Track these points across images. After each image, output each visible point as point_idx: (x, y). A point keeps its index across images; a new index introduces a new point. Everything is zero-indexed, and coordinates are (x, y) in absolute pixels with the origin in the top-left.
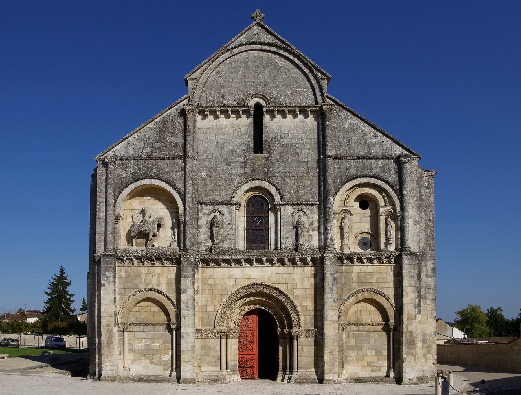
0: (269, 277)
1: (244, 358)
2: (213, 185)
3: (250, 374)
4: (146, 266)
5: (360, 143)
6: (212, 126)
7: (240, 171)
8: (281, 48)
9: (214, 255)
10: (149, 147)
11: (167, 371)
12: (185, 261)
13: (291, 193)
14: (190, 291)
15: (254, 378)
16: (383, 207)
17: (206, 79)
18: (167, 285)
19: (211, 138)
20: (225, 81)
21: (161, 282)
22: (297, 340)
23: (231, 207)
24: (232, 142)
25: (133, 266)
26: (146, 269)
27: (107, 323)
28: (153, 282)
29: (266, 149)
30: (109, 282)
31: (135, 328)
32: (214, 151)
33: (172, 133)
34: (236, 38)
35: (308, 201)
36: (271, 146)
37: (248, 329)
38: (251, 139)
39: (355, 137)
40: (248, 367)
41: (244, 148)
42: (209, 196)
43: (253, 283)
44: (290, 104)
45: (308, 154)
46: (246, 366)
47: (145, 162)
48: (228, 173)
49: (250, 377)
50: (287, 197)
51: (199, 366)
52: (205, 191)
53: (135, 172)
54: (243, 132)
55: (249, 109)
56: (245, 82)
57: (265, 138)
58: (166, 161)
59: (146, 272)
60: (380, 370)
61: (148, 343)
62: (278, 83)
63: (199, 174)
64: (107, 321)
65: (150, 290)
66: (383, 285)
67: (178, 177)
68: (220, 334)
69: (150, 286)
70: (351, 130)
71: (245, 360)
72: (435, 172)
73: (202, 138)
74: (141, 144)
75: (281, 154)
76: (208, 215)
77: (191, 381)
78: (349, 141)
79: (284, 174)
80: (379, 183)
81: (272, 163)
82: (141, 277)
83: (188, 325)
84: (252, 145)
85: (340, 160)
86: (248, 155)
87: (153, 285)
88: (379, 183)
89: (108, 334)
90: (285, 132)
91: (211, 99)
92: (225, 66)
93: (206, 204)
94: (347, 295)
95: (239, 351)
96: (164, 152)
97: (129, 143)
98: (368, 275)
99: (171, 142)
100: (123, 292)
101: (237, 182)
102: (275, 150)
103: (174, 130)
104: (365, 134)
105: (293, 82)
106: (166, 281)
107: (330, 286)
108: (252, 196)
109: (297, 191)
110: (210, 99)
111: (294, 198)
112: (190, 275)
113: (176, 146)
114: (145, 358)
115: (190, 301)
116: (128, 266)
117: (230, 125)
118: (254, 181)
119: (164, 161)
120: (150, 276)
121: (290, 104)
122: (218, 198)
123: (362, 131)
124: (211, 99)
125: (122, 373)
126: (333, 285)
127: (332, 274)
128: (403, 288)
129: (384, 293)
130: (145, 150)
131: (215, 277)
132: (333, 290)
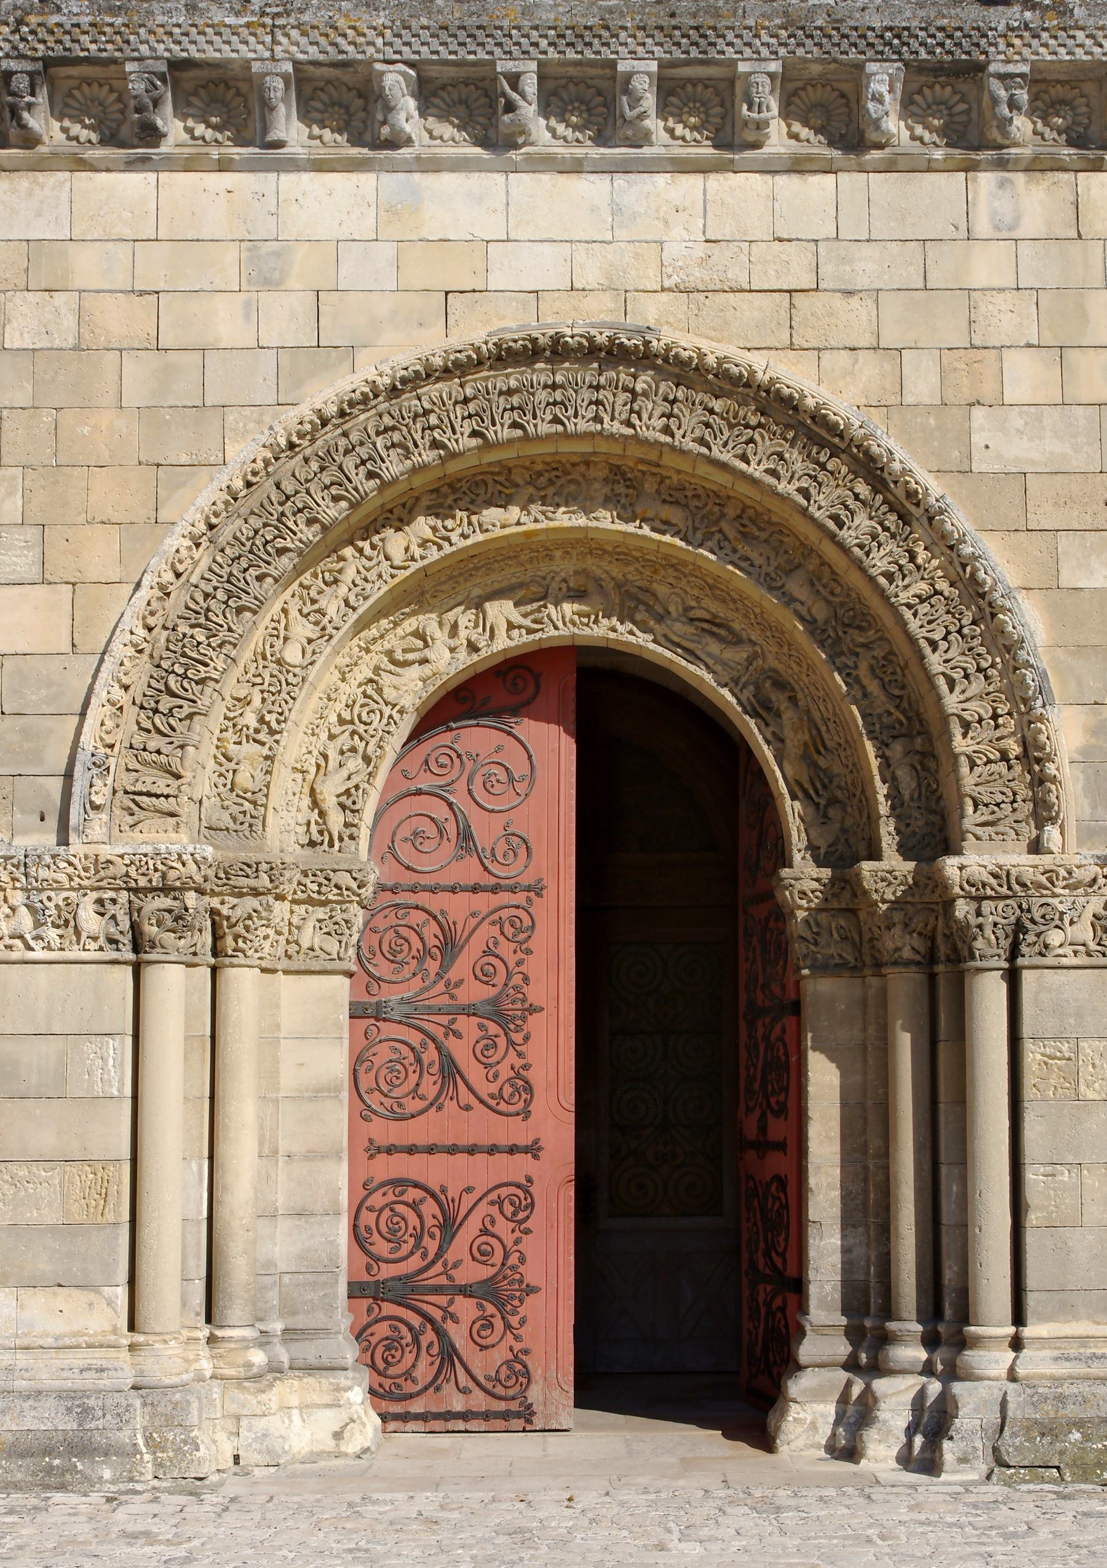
0: (698, 276)
1: (413, 1194)
3: (483, 1363)
37: (469, 871)
46: (434, 1276)
49: (479, 1401)
71: (430, 1208)
95: (362, 1113)
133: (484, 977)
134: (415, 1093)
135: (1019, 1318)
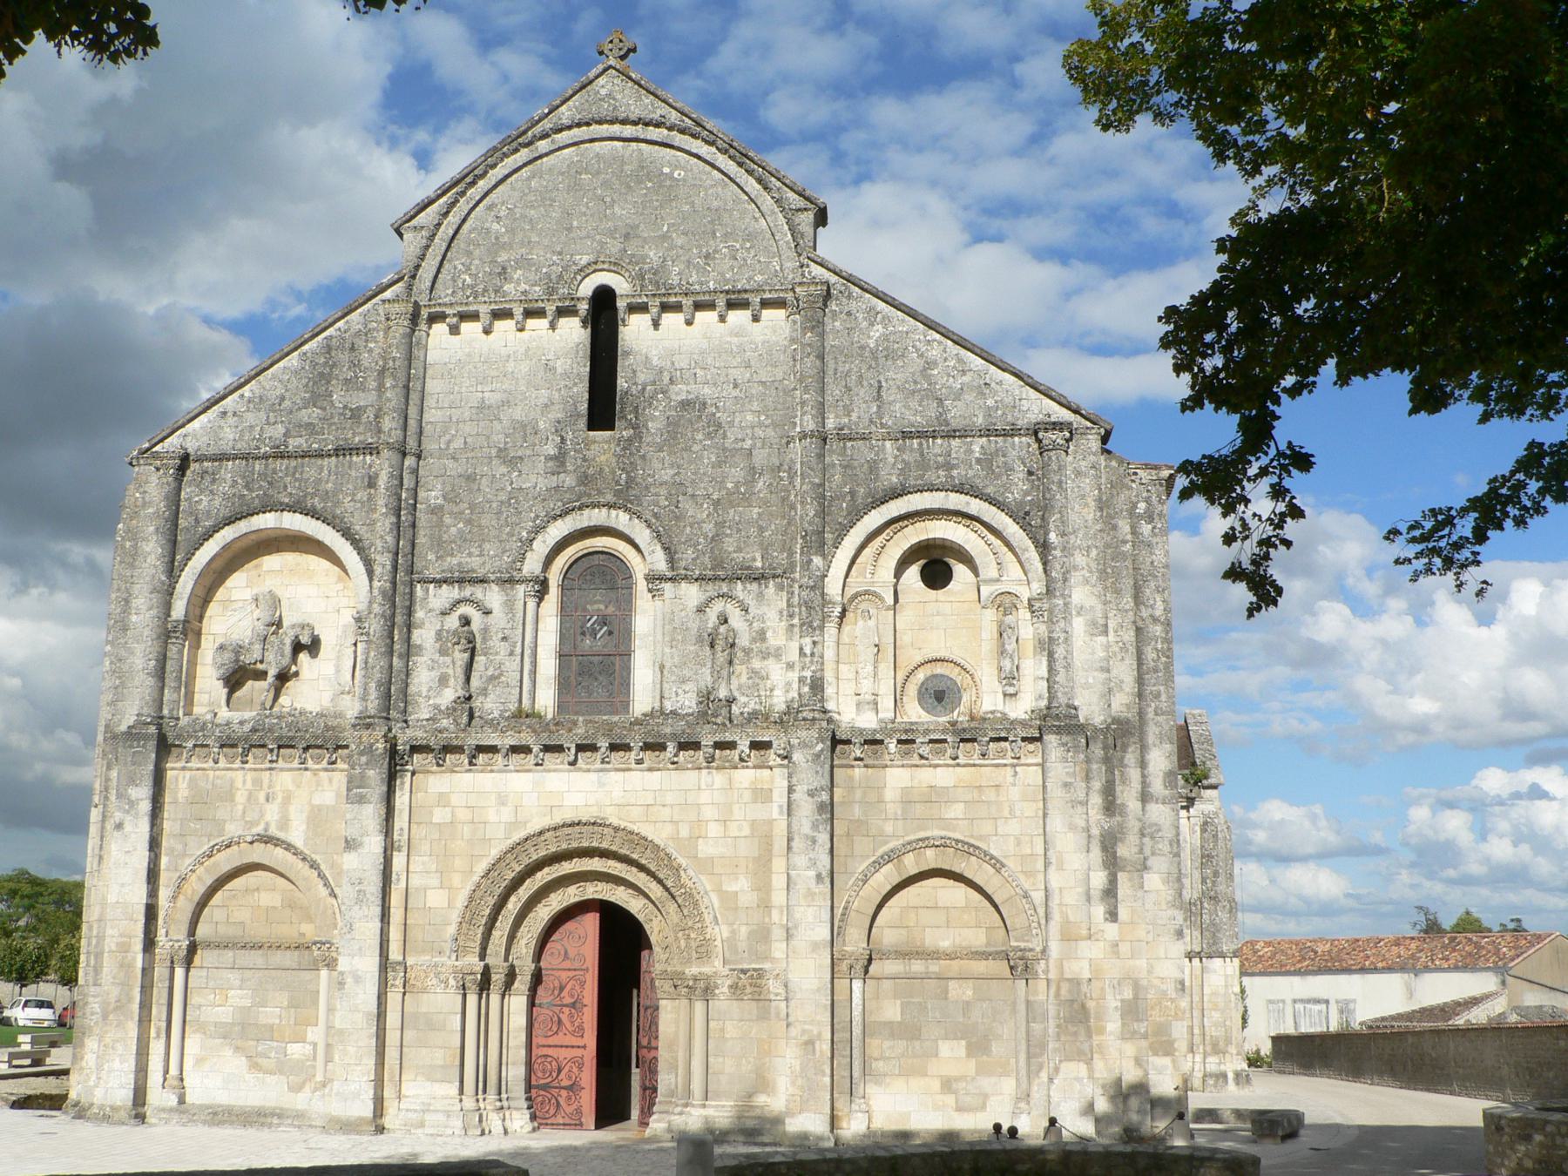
0: (622, 801)
2: (461, 525)
3: (569, 1110)
4: (250, 769)
6: (469, 355)
7: (543, 484)
8: (682, 131)
12: (361, 753)
19: (464, 389)
20: (511, 231)
23: (512, 589)
24: (526, 398)
26: (250, 775)
27: (120, 940)
28: (268, 817)
29: (624, 417)
30: (136, 816)
35: (749, 568)
36: (641, 408)
37: (567, 964)
42: (449, 559)
43: (569, 821)
44: (701, 284)
45: (753, 428)
46: (555, 1084)
47: (266, 466)
48: (509, 488)
49: (567, 1121)
54: (559, 370)
56: (570, 229)
57: (622, 383)
59: (249, 785)
61: (247, 1003)
62: (665, 228)
65: (257, 840)
66: (987, 828)
69: (259, 829)
71: (554, 1063)
73: (438, 390)
75: (673, 429)
78: (880, 387)
79: (678, 488)
80: (975, 506)
81: (643, 457)
82: (233, 801)
83: (360, 949)
85: (849, 444)
87: (267, 824)
89: (122, 974)
90: (684, 365)
91: (469, 281)
93: (439, 582)
94: (868, 857)
97: (224, 413)
98: (934, 797)
99: (345, 407)
101: (532, 515)
102: (653, 418)
104: (930, 364)
105: (712, 222)
109: (716, 539)
110: (464, 281)
111: (707, 560)
116: (198, 769)
117: (522, 350)
118: (586, 512)
119: (319, 462)
120: (262, 797)
121: (701, 284)
122: (474, 563)
126: (815, 826)
127: (811, 794)
131: (455, 800)
133: (572, 996)
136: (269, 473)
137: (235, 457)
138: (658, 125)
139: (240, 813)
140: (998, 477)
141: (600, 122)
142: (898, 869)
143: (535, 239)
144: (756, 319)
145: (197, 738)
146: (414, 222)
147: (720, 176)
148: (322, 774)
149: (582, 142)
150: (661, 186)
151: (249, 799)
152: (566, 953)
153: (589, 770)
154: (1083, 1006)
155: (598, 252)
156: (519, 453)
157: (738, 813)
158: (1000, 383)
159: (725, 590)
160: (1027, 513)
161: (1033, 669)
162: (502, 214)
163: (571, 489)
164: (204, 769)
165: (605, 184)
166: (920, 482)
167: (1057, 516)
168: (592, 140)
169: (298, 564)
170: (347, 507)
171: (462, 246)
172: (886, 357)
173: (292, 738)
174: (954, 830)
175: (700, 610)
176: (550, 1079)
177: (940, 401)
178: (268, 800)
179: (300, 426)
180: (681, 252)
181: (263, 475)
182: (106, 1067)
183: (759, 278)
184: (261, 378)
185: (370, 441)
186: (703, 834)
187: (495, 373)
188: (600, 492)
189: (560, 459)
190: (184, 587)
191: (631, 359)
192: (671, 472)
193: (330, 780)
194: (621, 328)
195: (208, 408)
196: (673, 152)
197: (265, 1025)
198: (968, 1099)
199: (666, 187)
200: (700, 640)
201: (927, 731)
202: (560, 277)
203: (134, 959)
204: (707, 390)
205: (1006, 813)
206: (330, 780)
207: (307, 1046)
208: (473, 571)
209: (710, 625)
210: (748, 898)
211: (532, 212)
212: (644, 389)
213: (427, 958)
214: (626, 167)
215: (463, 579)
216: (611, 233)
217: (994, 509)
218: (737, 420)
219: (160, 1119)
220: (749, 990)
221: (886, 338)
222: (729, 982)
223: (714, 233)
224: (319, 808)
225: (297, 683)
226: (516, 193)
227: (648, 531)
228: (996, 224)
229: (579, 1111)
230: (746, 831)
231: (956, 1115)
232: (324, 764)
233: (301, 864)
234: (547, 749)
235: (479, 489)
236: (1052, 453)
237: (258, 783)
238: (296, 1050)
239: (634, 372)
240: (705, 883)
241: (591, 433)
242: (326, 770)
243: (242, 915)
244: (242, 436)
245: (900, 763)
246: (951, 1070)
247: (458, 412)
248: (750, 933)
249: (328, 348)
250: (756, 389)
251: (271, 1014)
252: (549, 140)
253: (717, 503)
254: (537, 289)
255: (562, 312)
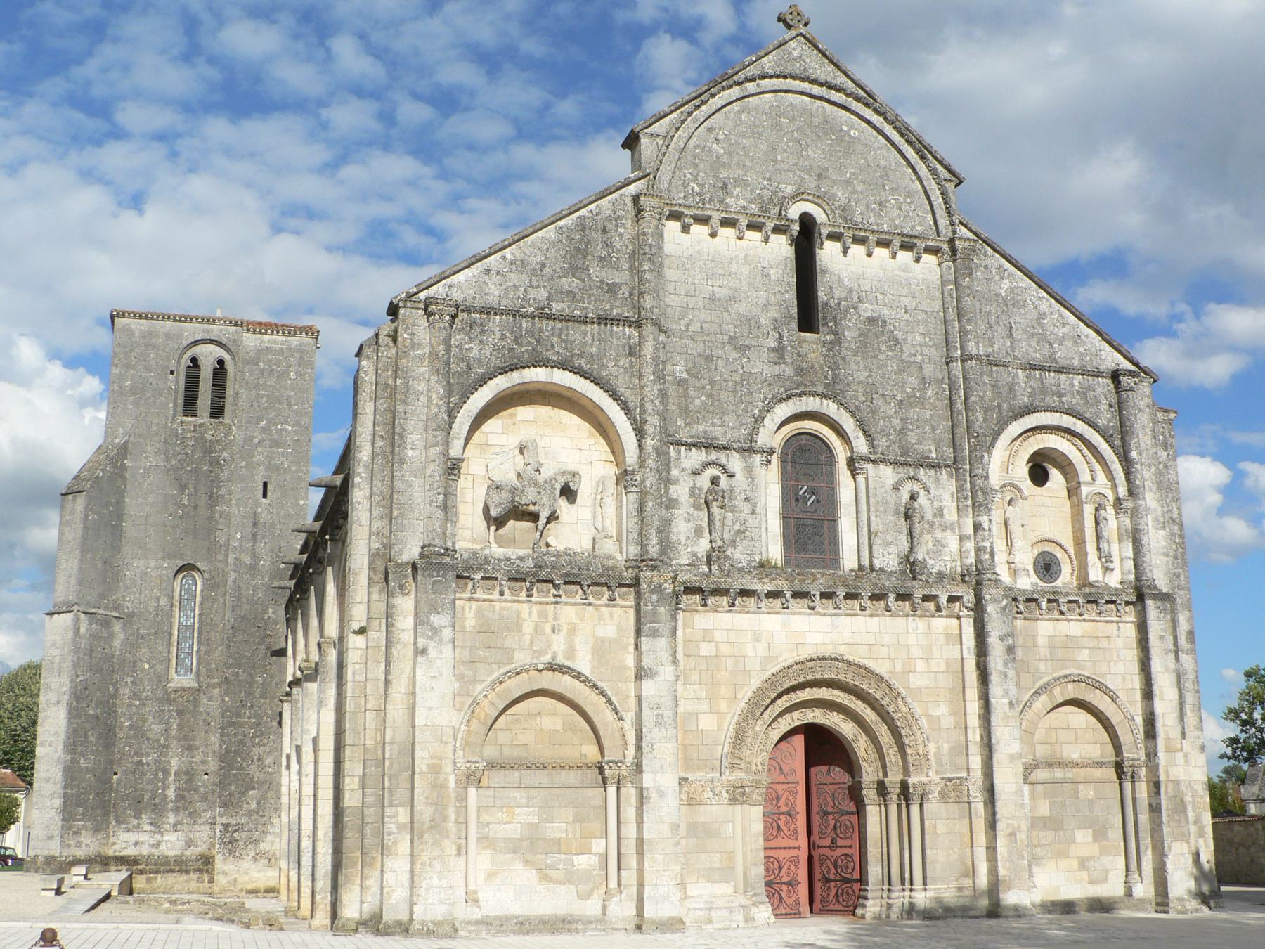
0: (851, 641)
1: (772, 860)
2: (703, 398)
3: (790, 901)
4: (536, 603)
5: (1033, 335)
6: (699, 253)
7: (769, 371)
8: (858, 99)
9: (717, 578)
10: (544, 286)
11: (588, 901)
12: (652, 592)
13: (890, 435)
14: (667, 672)
15: (798, 914)
16: (1088, 484)
17: (685, 140)
18: (593, 654)
19: (696, 281)
20: (729, 153)
21: (578, 647)
22: (921, 805)
23: (750, 457)
24: (748, 296)
25: (500, 601)
26: (535, 608)
27: (431, 762)
28: (555, 648)
29: (826, 324)
30: (440, 642)
31: (496, 778)
32: (703, 315)
33: (601, 259)
34: (754, 59)
35: (927, 458)
36: (838, 318)
37: (782, 779)
38: (791, 296)
39: (1021, 320)
40: (784, 883)
41: (776, 315)
42: (696, 426)
43: (815, 656)
44: (878, 225)
45: (921, 346)
46: (777, 880)
47: (533, 324)
48: (741, 371)
49: (789, 911)
50: (883, 443)
51: (682, 885)
52: (686, 412)
53: (507, 346)
54: (773, 277)
55: (788, 226)
56: (775, 161)
57: (822, 296)
58: (589, 328)
59: (535, 617)
60: (1105, 880)
61: (535, 820)
62: (848, 175)
63: (669, 367)
64: (432, 757)
65: (547, 669)
66: (1104, 668)
67: (622, 370)
68: (734, 792)
69: (547, 658)
70: (1012, 302)
71: (776, 863)
72: (1175, 412)
73: (675, 278)
74: (525, 276)
75: (863, 337)
76: (696, 473)
77: (673, 925)
78: (1011, 327)
79: (871, 388)
80: (1080, 427)
81: (844, 359)
82: (520, 631)
83: (662, 767)
84: (794, 311)
85: (994, 368)
86: (786, 334)
87: (554, 653)
88: (1080, 427)
89: (435, 795)
90: (867, 288)
91: (697, 189)
92: (727, 118)
93: (690, 446)
94: (1030, 689)
95: (766, 840)
96: (584, 303)
97: (488, 271)
98: (1069, 643)
99: (602, 281)
100: (470, 673)
101: (762, 396)
102: (849, 328)
103: (608, 252)
104: (1042, 316)
105: (881, 176)
106: (591, 645)
107: (1000, 666)
108: (793, 433)
109: (902, 432)
110: (693, 188)
111: (897, 449)
112: (665, 628)
113: (615, 292)
114: (525, 866)
115: (667, 702)
116: (485, 600)
117: (742, 256)
118: (804, 398)
119: (583, 327)
120: (548, 630)
121: (878, 225)
122: (718, 433)
123: (1036, 308)
124: (697, 189)
125: (465, 913)
126: (1005, 664)
127: (1002, 638)
128: (1153, 676)
129: (1109, 686)
130: (533, 294)
131: (718, 636)
132: (1006, 676)
133: (787, 805)
134: (771, 834)
135: (925, 883)
136: (537, 331)
137: (502, 313)
138: (838, 90)
139: (528, 642)
140: (1091, 406)
141: (794, 78)
142: (1050, 698)
143: (748, 164)
144: (918, 260)
145: (486, 571)
146: (649, 130)
147: (884, 141)
148: (604, 609)
149: (780, 91)
150: (842, 140)
151: (536, 630)
152: (781, 769)
153: (825, 615)
154: (1182, 800)
155: (799, 185)
156: (747, 343)
157: (936, 653)
158: (1087, 336)
159: (912, 474)
160: (1111, 436)
161: (1121, 552)
162: (720, 137)
163: (790, 378)
164: (491, 601)
165: (799, 129)
166: (1042, 404)
167: (1136, 440)
168: (787, 91)
169: (551, 418)
170: (613, 370)
171: (689, 158)
172: (1013, 304)
173: (578, 575)
174: (1084, 670)
175: (896, 488)
176: (773, 877)
177: (1051, 344)
178: (554, 632)
179: (562, 293)
180: (861, 196)
181: (530, 333)
182: (424, 884)
183: (918, 228)
184: (521, 243)
185: (627, 314)
186: (913, 670)
187: (721, 272)
188: (813, 384)
189: (779, 351)
190: (460, 428)
191: (827, 278)
192: (866, 374)
193: (611, 615)
194: (818, 251)
195: (473, 263)
196: (848, 114)
197: (553, 839)
198: (1095, 874)
199: (846, 144)
200: (897, 512)
201: (1067, 594)
202: (771, 199)
203: (446, 780)
204: (886, 312)
205: (1115, 658)
206: (611, 615)
207: (593, 857)
208: (716, 439)
209: (904, 501)
210: (948, 721)
211: (744, 141)
212: (840, 303)
213: (702, 774)
214: (815, 119)
215: (709, 445)
216: (808, 170)
217: (1091, 429)
218: (909, 339)
219: (469, 932)
220: (953, 794)
221: (1011, 290)
222: (939, 789)
223: (884, 186)
224: (603, 640)
225: (558, 526)
226: (730, 123)
227: (852, 420)
228: (292, 223)
229: (797, 902)
230: (943, 668)
231: (1089, 886)
232: (605, 600)
233: (588, 691)
234: (796, 595)
235: (716, 369)
236: (1129, 393)
237: (543, 615)
238: (582, 862)
239: (831, 288)
240: (918, 710)
241: (802, 334)
242: (608, 606)
243: (526, 737)
244: (507, 294)
245: (1047, 617)
246: (1084, 852)
247: (694, 300)
248: (950, 750)
249: (582, 226)
250: (921, 316)
251: (557, 829)
252: (755, 83)
253: (901, 403)
254: (754, 206)
255: (777, 230)
